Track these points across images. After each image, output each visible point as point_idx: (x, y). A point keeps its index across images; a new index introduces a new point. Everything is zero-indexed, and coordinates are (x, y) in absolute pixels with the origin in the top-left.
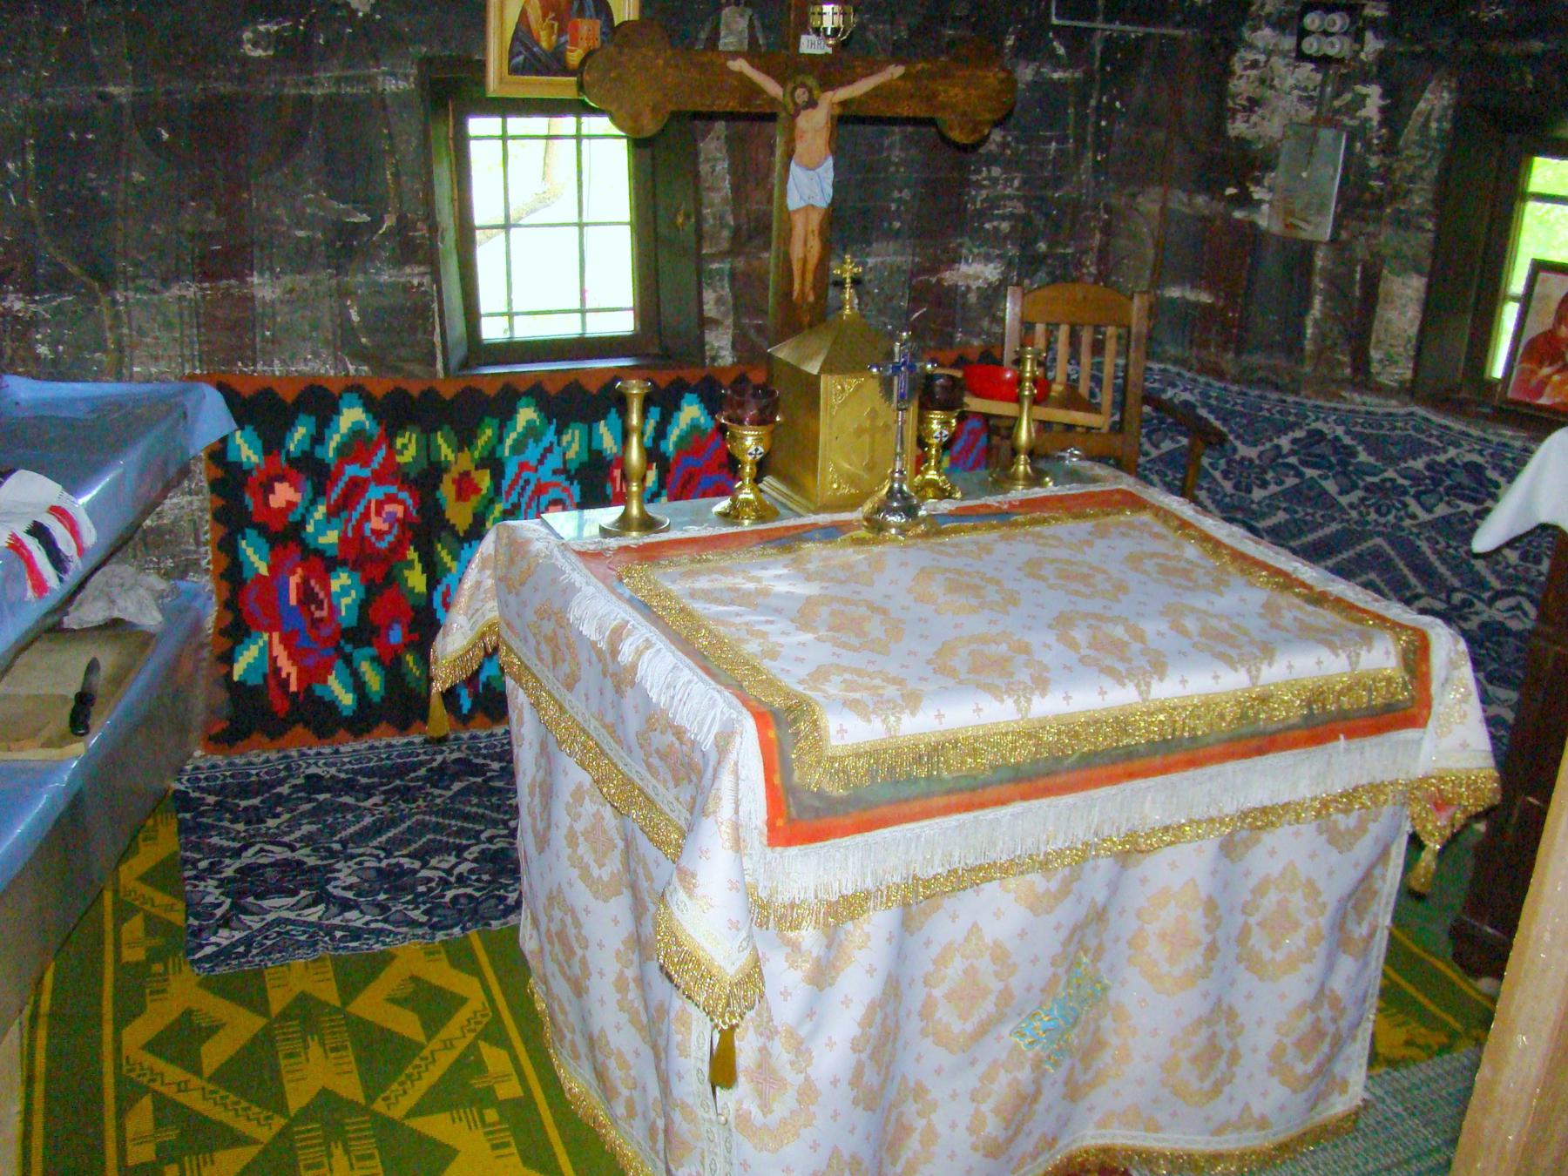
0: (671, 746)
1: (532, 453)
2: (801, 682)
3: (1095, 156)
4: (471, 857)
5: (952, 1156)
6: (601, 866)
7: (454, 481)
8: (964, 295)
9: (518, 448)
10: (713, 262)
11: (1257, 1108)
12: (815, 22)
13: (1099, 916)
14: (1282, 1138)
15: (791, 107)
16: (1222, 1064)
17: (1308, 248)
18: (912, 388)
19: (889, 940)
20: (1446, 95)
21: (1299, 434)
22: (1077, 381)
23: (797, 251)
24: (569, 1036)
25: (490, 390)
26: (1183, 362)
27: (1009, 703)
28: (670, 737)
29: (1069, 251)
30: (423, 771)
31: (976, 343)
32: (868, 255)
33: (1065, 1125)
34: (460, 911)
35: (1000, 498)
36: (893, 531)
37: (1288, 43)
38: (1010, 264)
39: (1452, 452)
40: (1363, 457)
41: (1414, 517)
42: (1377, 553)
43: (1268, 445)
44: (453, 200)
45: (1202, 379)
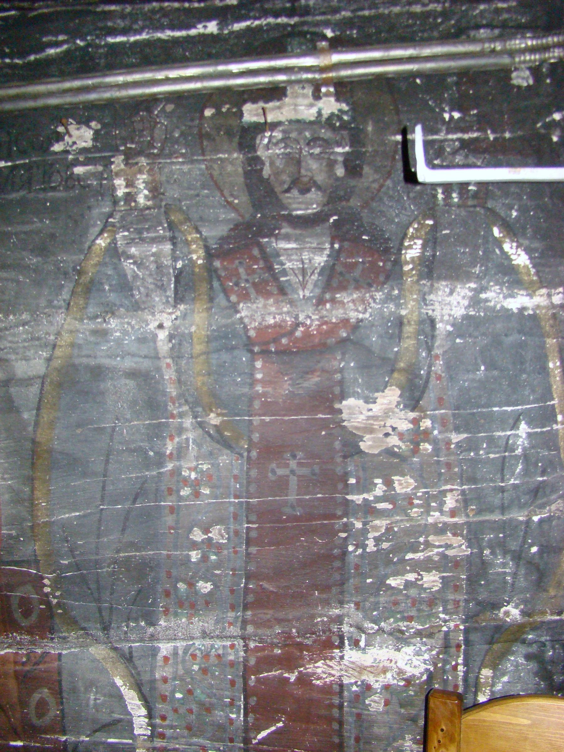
8: (358, 698)
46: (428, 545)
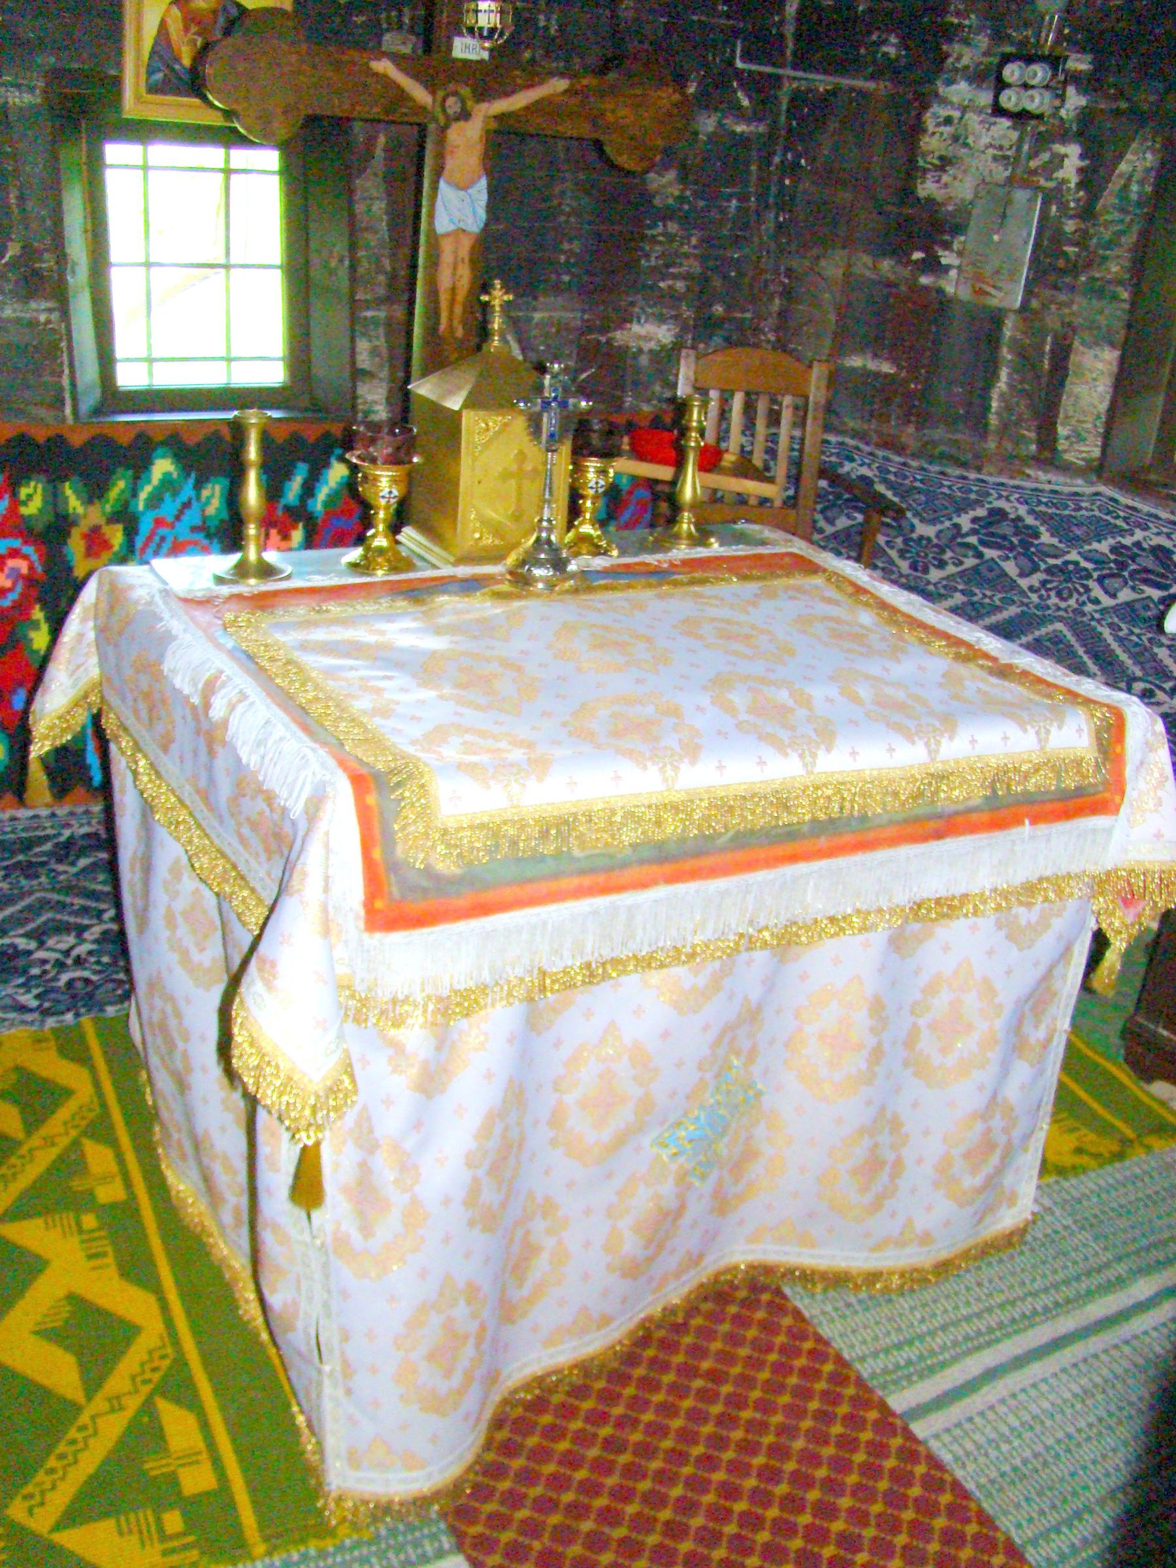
0: (261, 814)
1: (169, 509)
2: (413, 742)
3: (777, 217)
4: (92, 938)
5: (586, 1276)
6: (202, 950)
7: (85, 536)
8: (635, 357)
9: (155, 501)
10: (368, 308)
11: (922, 1222)
12: (469, 20)
13: (752, 1015)
14: (944, 1255)
15: (442, 121)
16: (884, 1177)
17: (996, 318)
18: (564, 430)
19: (510, 1041)
20: (1149, 156)
21: (981, 512)
22: (751, 453)
23: (445, 279)
24: (176, 1136)
25: (124, 439)
26: (862, 436)
27: (653, 770)
28: (261, 805)
29: (748, 315)
30: (48, 847)
31: (646, 408)
32: (535, 309)
33: (713, 1239)
34: (74, 997)
35: (659, 556)
36: (540, 586)
37: (985, 98)
38: (684, 328)
39: (1139, 535)
40: (1046, 538)
41: (1096, 602)
42: (1057, 639)
43: (947, 524)
44: (86, 231)
45: (881, 453)
46: (681, 265)
